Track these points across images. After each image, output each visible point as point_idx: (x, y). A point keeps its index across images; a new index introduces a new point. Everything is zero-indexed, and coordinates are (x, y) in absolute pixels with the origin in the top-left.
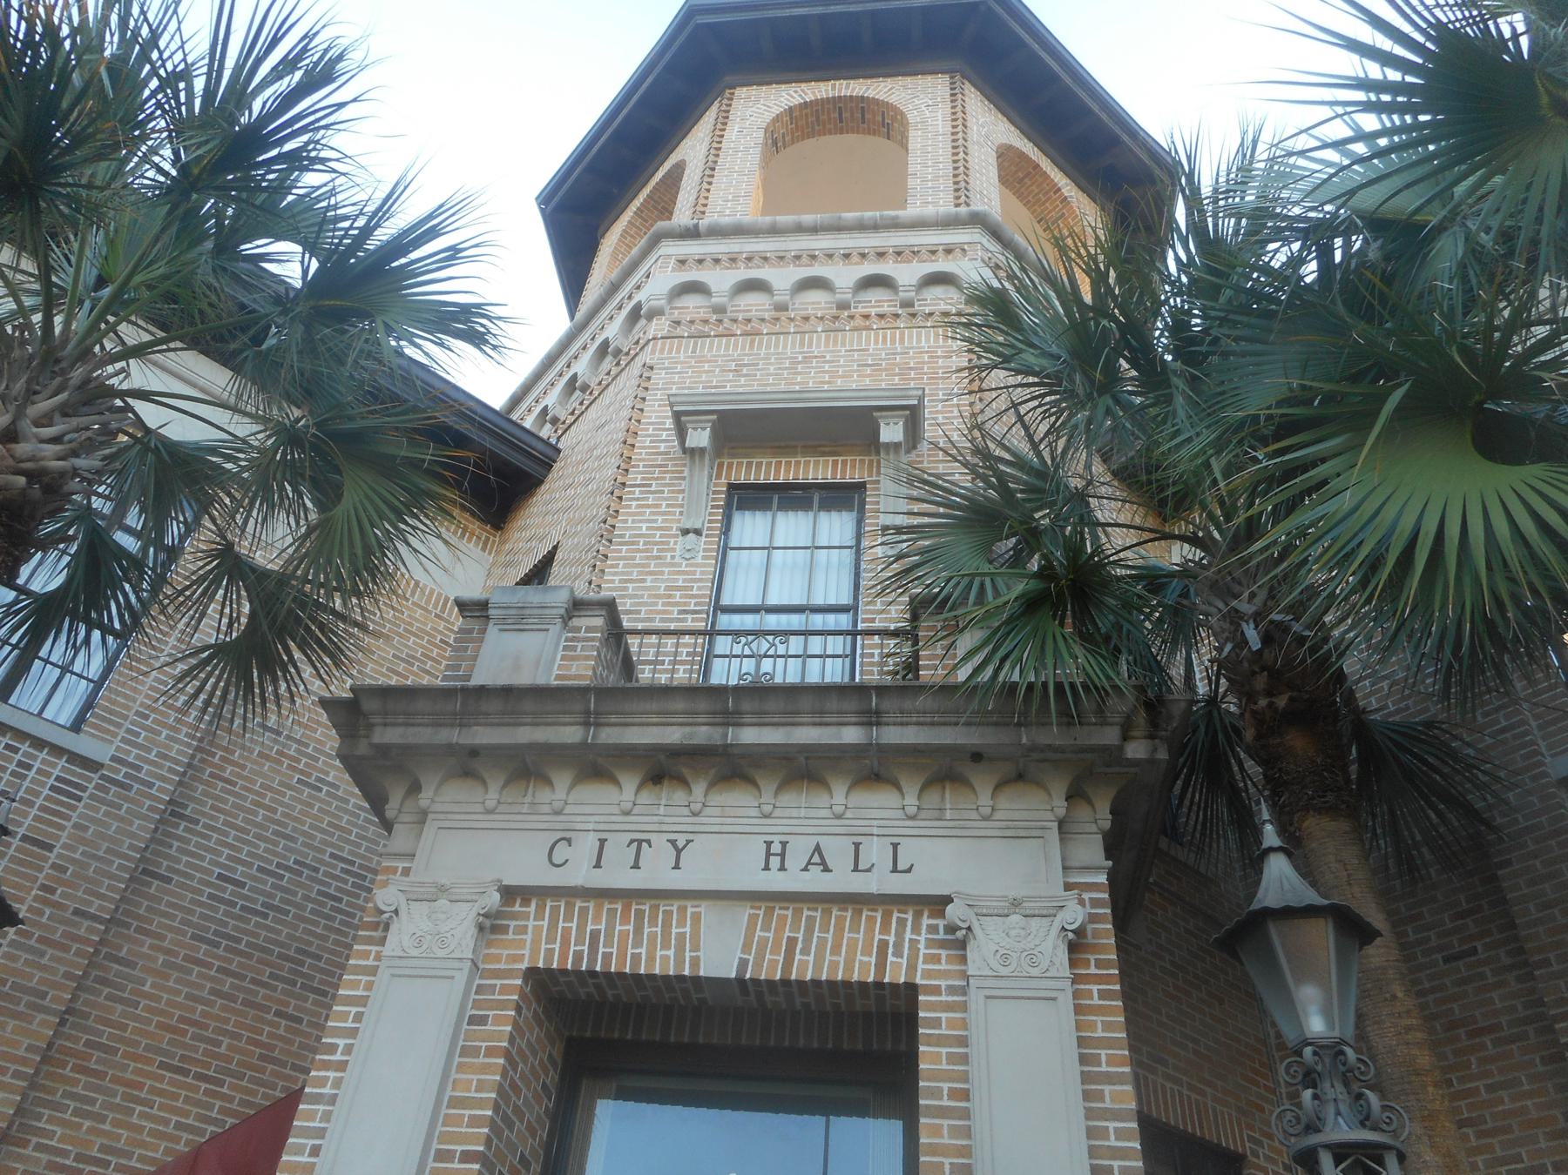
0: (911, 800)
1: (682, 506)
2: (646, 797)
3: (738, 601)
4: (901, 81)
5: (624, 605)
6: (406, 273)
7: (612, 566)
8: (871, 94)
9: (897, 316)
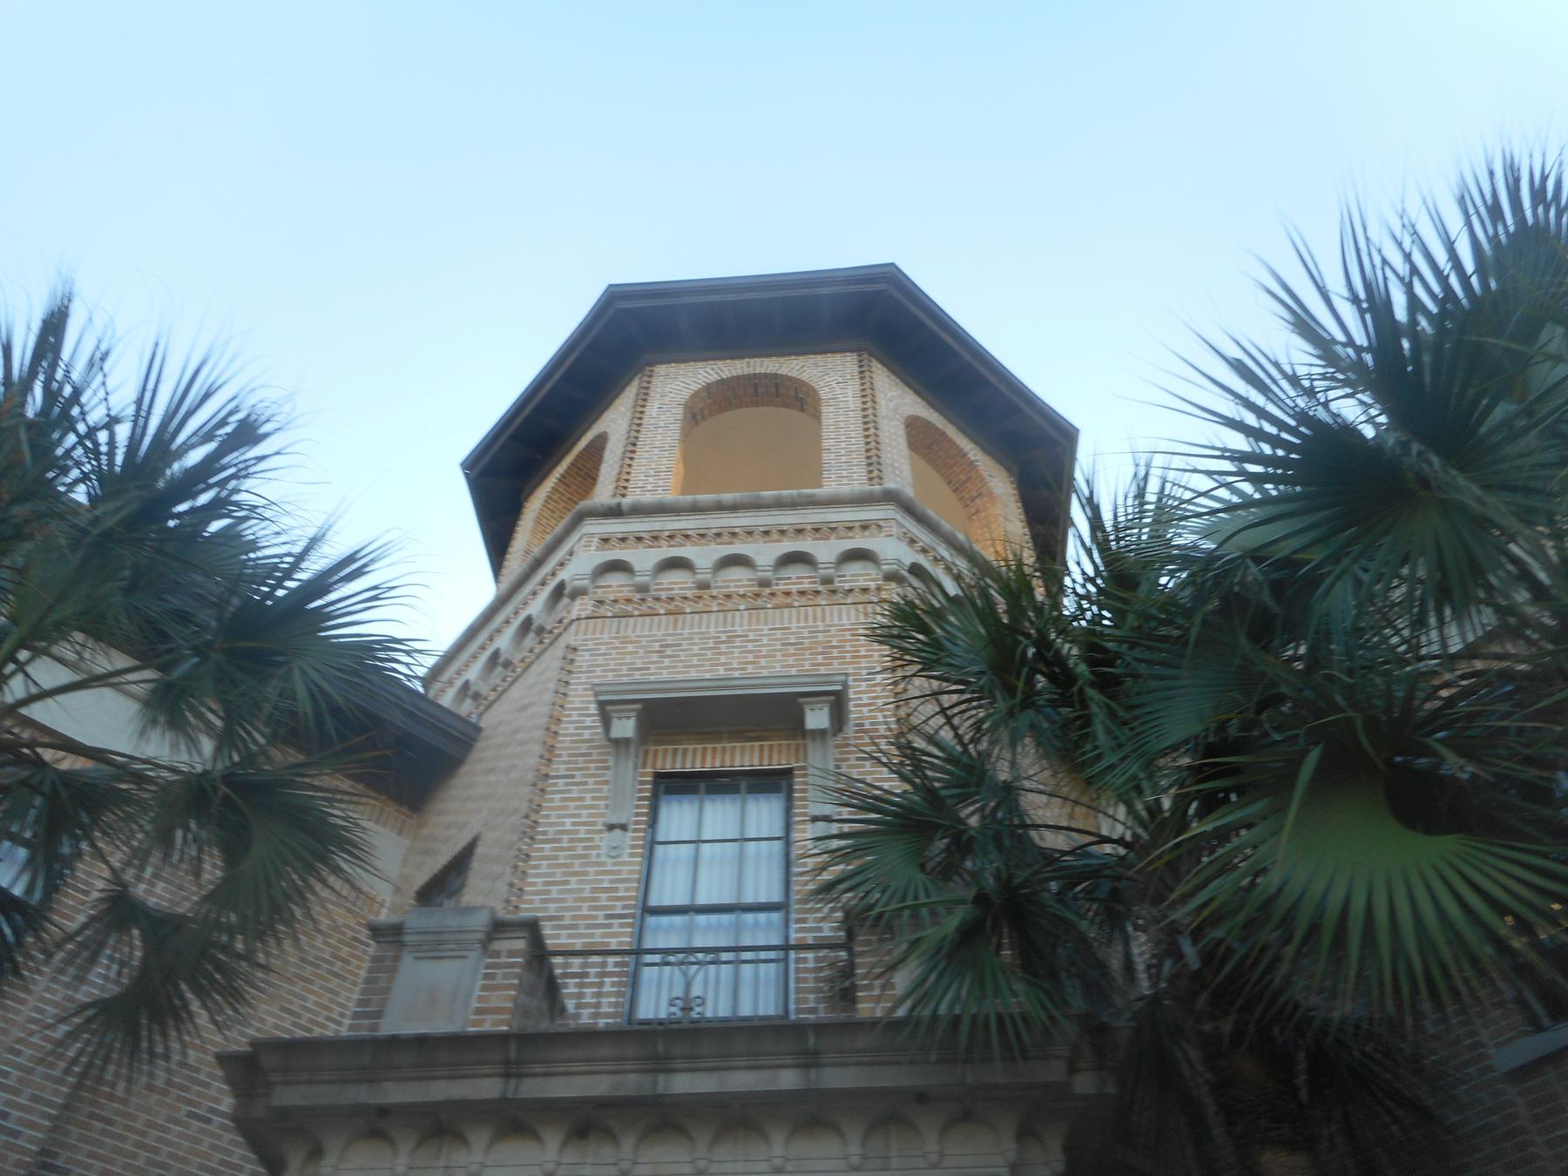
0: (854, 1149)
1: (606, 798)
2: (571, 1155)
3: (666, 902)
4: (812, 359)
5: (547, 930)
6: (322, 616)
7: (535, 867)
8: (784, 371)
9: (817, 592)
